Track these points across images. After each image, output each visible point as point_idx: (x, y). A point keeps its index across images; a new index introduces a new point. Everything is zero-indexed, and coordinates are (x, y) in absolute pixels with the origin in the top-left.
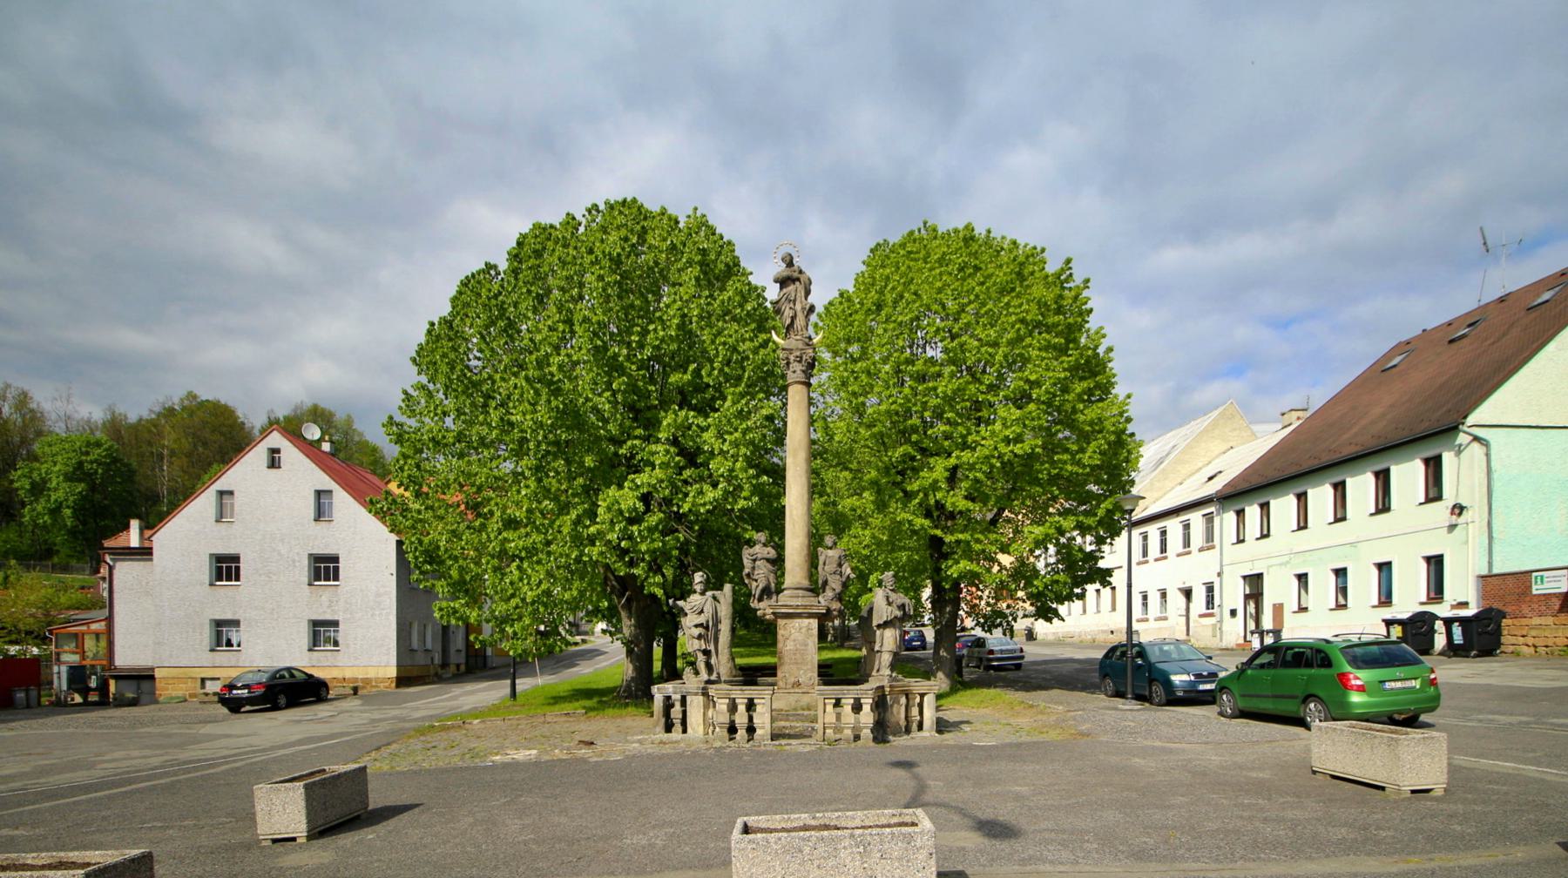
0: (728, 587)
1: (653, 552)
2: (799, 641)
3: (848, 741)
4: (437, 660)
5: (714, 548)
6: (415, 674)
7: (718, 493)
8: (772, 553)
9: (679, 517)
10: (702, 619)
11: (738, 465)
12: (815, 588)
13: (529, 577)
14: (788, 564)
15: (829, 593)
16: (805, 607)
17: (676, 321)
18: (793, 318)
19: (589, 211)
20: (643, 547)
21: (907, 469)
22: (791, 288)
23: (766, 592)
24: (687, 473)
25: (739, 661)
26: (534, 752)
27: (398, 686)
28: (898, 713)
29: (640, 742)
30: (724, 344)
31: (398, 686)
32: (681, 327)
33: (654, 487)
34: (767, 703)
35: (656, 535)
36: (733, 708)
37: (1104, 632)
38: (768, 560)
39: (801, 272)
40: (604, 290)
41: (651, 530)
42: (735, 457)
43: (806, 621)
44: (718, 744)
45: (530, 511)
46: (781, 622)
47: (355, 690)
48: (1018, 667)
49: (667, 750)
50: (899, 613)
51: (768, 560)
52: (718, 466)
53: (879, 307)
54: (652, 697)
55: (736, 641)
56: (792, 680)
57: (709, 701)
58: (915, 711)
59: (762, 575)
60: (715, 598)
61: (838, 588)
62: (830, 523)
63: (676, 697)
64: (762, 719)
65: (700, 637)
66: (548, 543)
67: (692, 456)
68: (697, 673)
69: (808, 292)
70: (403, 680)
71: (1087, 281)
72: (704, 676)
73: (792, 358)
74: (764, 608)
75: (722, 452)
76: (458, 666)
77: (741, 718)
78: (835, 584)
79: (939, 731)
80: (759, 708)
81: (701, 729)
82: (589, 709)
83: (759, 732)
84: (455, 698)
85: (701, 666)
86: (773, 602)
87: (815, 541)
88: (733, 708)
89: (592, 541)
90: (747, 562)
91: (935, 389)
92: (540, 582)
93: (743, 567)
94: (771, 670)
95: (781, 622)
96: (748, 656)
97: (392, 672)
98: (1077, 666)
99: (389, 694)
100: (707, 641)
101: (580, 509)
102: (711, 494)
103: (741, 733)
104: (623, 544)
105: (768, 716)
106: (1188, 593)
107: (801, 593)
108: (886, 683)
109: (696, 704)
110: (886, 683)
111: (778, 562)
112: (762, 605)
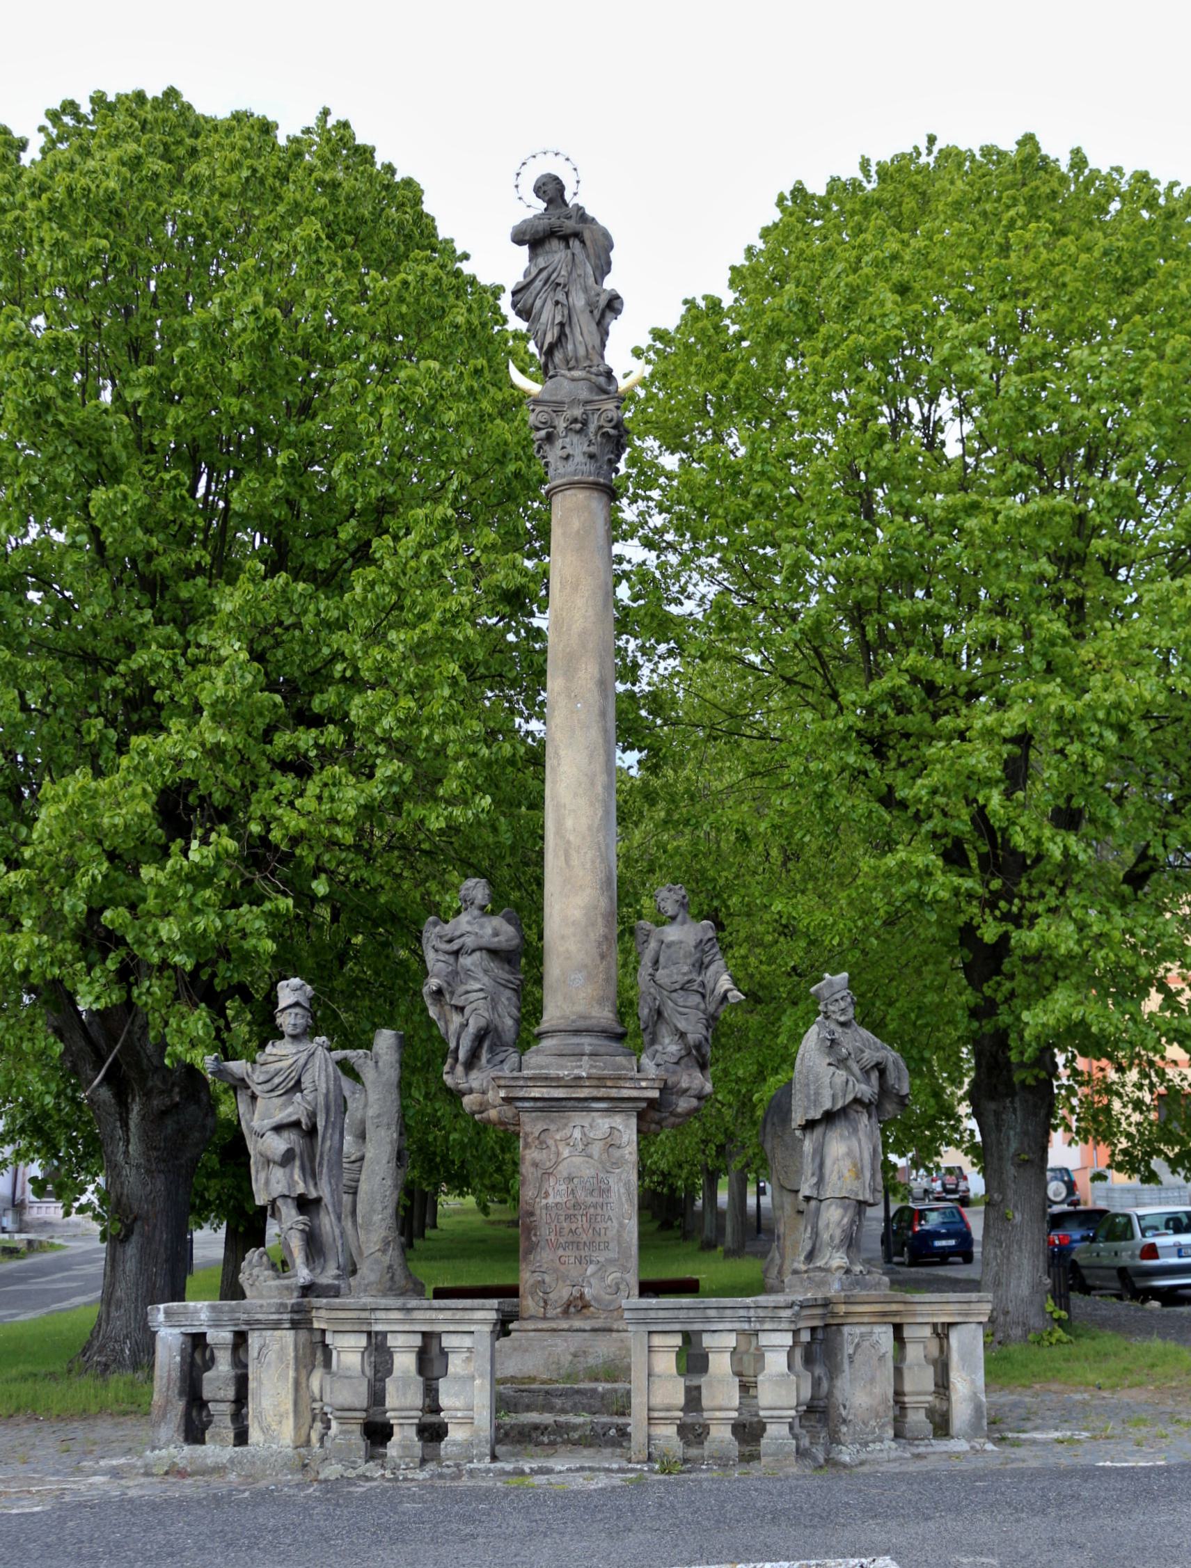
0: (385, 1039)
10: (295, 1110)
12: (628, 1027)
14: (554, 969)
16: (600, 1081)
29: (115, 1473)
38: (493, 953)
44: (332, 1471)
46: (531, 1126)
50: (867, 1090)
51: (493, 953)
56: (563, 1293)
59: (469, 998)
60: (346, 1068)
63: (220, 1337)
64: (467, 1400)
65: (287, 1159)
69: (604, 268)
73: (561, 424)
74: (481, 1089)
77: (403, 1398)
80: (456, 1364)
81: (286, 1433)
83: (456, 1434)
88: (378, 1349)
103: (404, 1437)
107: (587, 1043)
109: (273, 1355)
111: (523, 960)
112: (476, 1079)
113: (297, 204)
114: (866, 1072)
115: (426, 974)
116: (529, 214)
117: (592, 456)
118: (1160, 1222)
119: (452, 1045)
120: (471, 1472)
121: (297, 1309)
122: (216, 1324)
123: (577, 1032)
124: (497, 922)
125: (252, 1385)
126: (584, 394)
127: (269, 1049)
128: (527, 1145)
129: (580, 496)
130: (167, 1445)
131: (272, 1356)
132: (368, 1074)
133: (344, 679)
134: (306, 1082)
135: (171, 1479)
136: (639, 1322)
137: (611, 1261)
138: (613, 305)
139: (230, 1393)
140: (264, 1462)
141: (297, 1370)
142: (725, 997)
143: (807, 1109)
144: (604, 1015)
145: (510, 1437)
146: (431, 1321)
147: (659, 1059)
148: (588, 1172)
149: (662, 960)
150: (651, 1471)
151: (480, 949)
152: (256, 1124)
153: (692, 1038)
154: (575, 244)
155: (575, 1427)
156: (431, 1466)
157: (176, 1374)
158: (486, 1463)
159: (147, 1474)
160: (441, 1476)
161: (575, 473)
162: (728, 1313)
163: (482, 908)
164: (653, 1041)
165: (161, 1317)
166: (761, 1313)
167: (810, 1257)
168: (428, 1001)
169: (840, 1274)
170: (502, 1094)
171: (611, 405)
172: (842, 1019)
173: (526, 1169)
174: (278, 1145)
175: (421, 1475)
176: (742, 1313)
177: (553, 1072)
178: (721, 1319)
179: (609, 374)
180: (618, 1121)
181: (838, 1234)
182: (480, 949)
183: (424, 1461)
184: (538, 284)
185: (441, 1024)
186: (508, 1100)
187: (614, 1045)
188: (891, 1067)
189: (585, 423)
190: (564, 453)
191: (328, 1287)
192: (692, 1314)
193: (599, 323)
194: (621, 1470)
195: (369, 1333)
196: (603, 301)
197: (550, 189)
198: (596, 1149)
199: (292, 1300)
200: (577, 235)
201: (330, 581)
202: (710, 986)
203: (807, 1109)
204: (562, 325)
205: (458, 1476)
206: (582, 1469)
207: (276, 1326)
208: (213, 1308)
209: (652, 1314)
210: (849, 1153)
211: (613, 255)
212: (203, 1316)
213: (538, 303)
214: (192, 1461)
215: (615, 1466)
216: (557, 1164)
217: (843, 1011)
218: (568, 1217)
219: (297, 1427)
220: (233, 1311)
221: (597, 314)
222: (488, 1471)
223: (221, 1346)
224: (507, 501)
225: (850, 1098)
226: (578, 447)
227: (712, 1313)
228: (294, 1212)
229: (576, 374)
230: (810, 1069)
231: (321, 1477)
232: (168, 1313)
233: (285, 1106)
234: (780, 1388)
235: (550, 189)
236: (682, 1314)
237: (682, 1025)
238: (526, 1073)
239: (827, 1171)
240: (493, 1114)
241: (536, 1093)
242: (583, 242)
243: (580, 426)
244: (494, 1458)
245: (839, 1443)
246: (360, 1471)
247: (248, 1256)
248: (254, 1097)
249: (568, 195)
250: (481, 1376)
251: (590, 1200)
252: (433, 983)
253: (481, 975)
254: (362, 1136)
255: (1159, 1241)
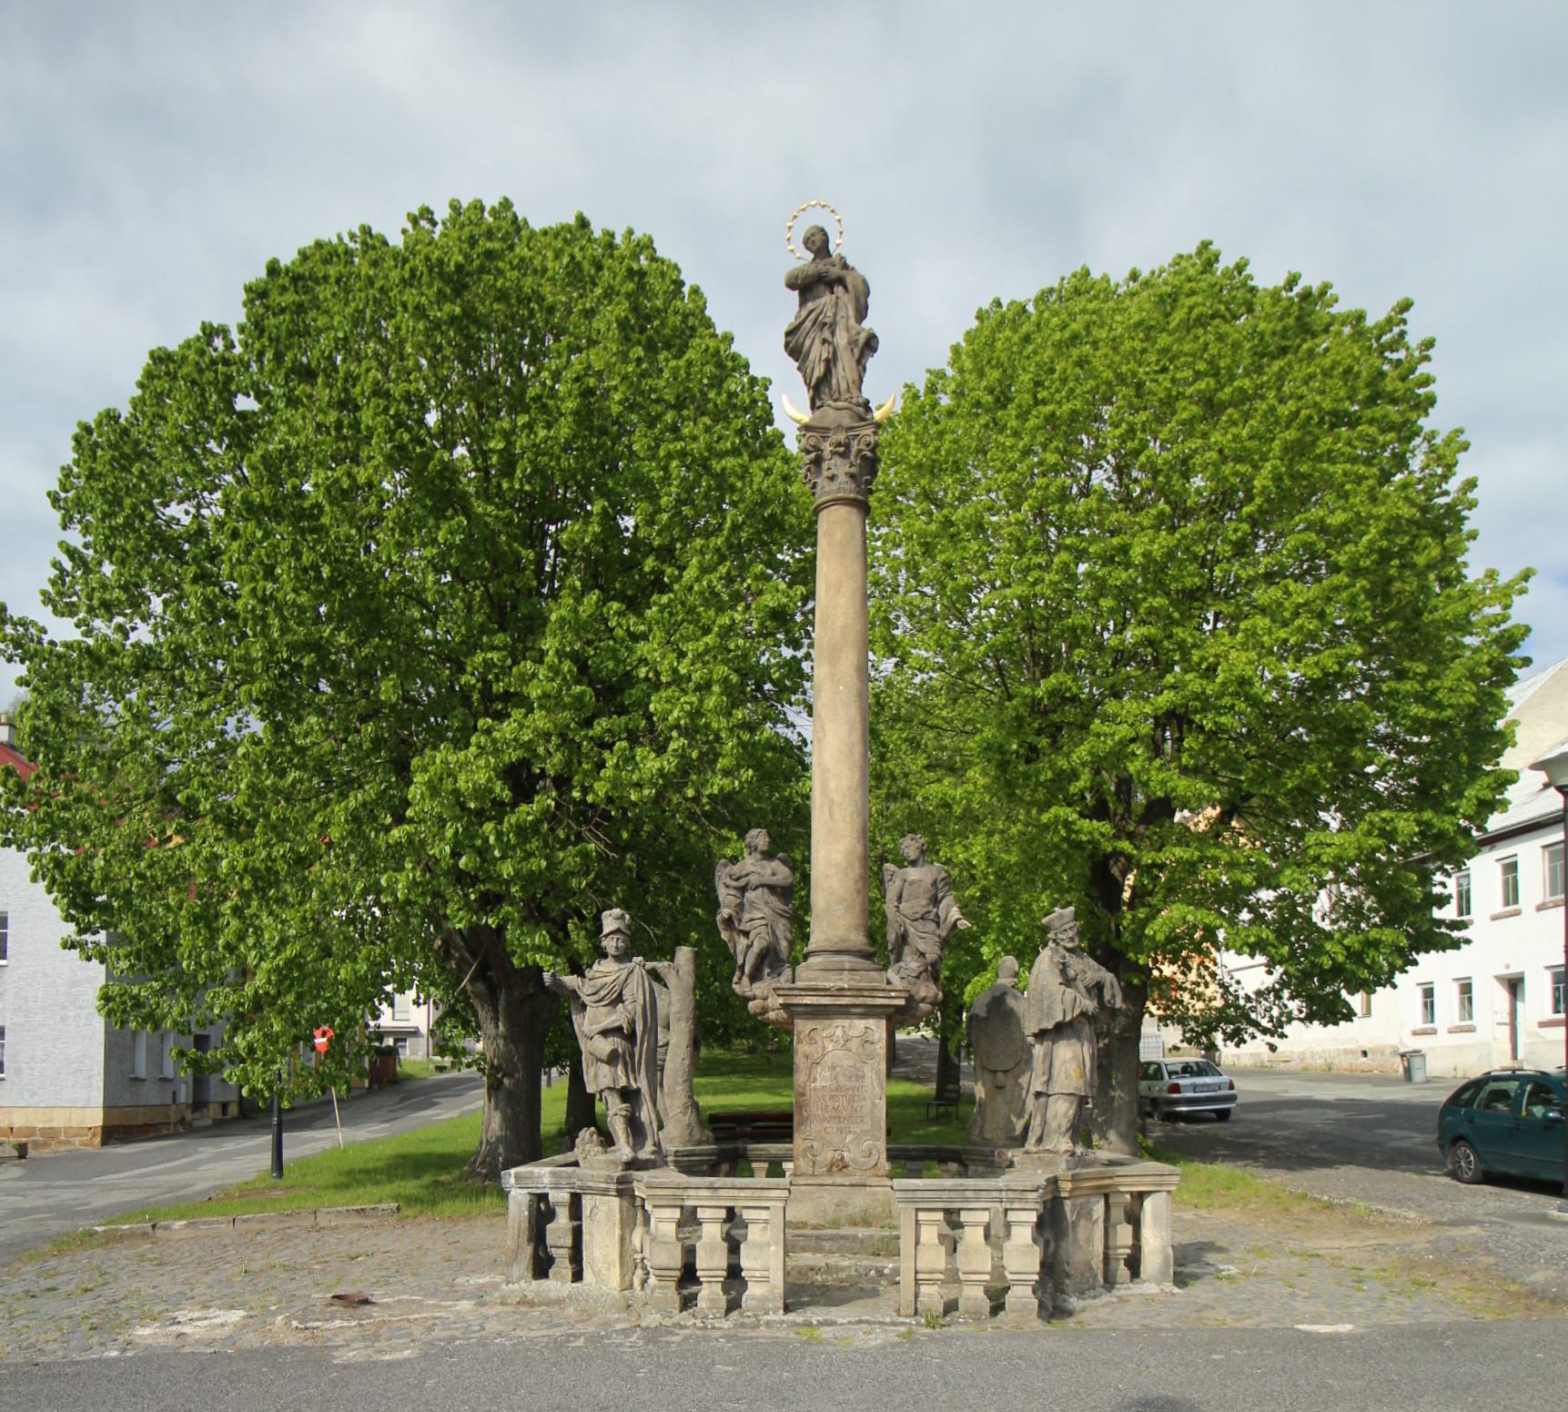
0: (684, 954)
1: (529, 880)
2: (845, 1071)
3: (975, 1315)
4: (185, 1096)
5: (661, 875)
6: (141, 1121)
7: (669, 763)
8: (778, 872)
9: (584, 813)
10: (618, 1017)
11: (711, 702)
12: (879, 945)
13: (259, 932)
14: (819, 899)
15: (911, 963)
16: (859, 991)
17: (570, 405)
18: (830, 363)
19: (415, 221)
20: (507, 869)
21: (1055, 721)
22: (827, 299)
23: (769, 960)
24: (601, 725)
25: (709, 1101)
26: (236, 1316)
27: (104, 1143)
28: (1087, 1243)
29: (480, 1297)
30: (683, 454)
31: (104, 1143)
32: (584, 417)
33: (528, 746)
34: (770, 1218)
35: (535, 844)
36: (689, 1219)
37: (1346, 1052)
38: (772, 888)
39: (845, 266)
40: (428, 334)
41: (523, 832)
42: (704, 687)
43: (860, 1024)
44: (652, 1319)
45: (256, 791)
46: (802, 1026)
47: (22, 1150)
48: (1223, 1115)
49: (534, 1331)
50: (1090, 1005)
51: (772, 888)
52: (669, 707)
53: (1003, 401)
54: (503, 1194)
55: (700, 1067)
56: (829, 1155)
57: (634, 1211)
58: (1124, 1234)
59: (760, 922)
60: (655, 975)
61: (932, 953)
62: (895, 820)
63: (560, 1197)
64: (765, 1262)
65: (612, 1059)
66: (302, 862)
67: (613, 691)
68: (607, 1140)
69: (862, 313)
70: (114, 1132)
71: (1429, 344)
72: (624, 1150)
73: (827, 448)
74: (764, 996)
75: (678, 680)
76: (225, 1106)
77: (711, 1260)
78: (925, 942)
79: (1180, 1280)
80: (754, 1233)
81: (614, 1277)
82: (411, 1200)
83: (754, 1290)
84: (194, 1166)
85: (618, 1128)
86: (783, 981)
87: (875, 863)
88: (689, 1219)
89: (395, 858)
90: (724, 894)
91: (1124, 550)
92: (283, 942)
93: (714, 904)
94: (779, 1126)
95: (802, 1026)
96: (727, 1092)
97: (96, 1118)
98: (1332, 1114)
99: (90, 1156)
100: (631, 1068)
101: (370, 791)
102: (651, 764)
103: (710, 1292)
104: (463, 862)
105: (776, 1251)
106: (1514, 985)
107: (847, 961)
108: (1061, 1169)
109: (603, 1215)
110: (1061, 1169)
111: (794, 898)
112: (759, 988)
113: (611, 287)
114: (1088, 990)
115: (718, 906)
116: (800, 264)
117: (852, 476)
118: (1179, 1068)
119: (740, 961)
120: (768, 1324)
121: (620, 1181)
122: (556, 1187)
123: (839, 952)
124: (776, 864)
125: (585, 1237)
126: (847, 422)
127: (596, 967)
128: (800, 1041)
129: (842, 512)
130: (519, 1280)
131: (601, 1215)
132: (671, 980)
133: (647, 679)
134: (627, 995)
135: (523, 1309)
136: (907, 1201)
137: (865, 1132)
138: (870, 344)
139: (569, 1241)
140: (596, 1300)
141: (622, 1228)
142: (955, 925)
143: (1040, 1020)
144: (858, 940)
145: (798, 1294)
146: (734, 1198)
147: (903, 973)
148: (847, 1063)
149: (905, 895)
150: (918, 1324)
151: (763, 886)
152: (586, 1028)
153: (931, 957)
154: (839, 290)
155: (842, 1269)
156: (735, 1315)
157: (525, 1225)
158: (780, 1316)
159: (503, 1304)
160: (743, 1325)
161: (839, 490)
162: (984, 1194)
163: (763, 853)
164: (899, 959)
165: (512, 1180)
166: (1011, 1195)
167: (1040, 1140)
168: (721, 927)
169: (1066, 1157)
170: (781, 1001)
171: (869, 431)
172: (1070, 945)
173: (799, 1060)
174: (605, 1046)
175: (726, 1324)
176: (995, 1194)
177: (821, 984)
178: (978, 1200)
179: (866, 405)
180: (871, 1022)
181: (1065, 1124)
182: (763, 886)
183: (729, 1310)
184: (808, 324)
185: (730, 945)
186: (785, 1006)
187: (867, 963)
188: (1108, 985)
189: (848, 446)
190: (829, 474)
191: (647, 1161)
192: (953, 1194)
193: (859, 362)
194: (894, 1324)
195: (682, 1207)
196: (862, 338)
197: (819, 244)
198: (854, 1044)
199: (618, 1173)
200: (841, 281)
201: (635, 604)
202: (942, 916)
203: (1040, 1020)
204: (827, 361)
205: (756, 1326)
206: (860, 1322)
207: (604, 1192)
208: (554, 1174)
209: (919, 1194)
210: (1074, 1058)
211: (870, 300)
212: (546, 1181)
213: (808, 342)
214: (538, 1294)
215: (888, 1320)
216: (823, 1056)
217: (1072, 939)
218: (832, 1097)
219: (623, 1276)
220: (569, 1177)
221: (857, 352)
222: (782, 1322)
223: (561, 1204)
224: (779, 531)
225: (1077, 1012)
226: (840, 468)
227: (969, 1194)
228: (617, 1100)
229: (840, 404)
230: (1044, 987)
231: (643, 1324)
232: (517, 1177)
233: (609, 1014)
234: (1023, 1255)
235: (819, 244)
236: (944, 1195)
237: (922, 947)
238: (799, 984)
239: (1055, 1072)
240: (772, 1015)
241: (807, 1000)
242: (845, 288)
243: (843, 451)
244: (787, 1309)
245: (1063, 1292)
246: (676, 1319)
247: (581, 1134)
248: (584, 1006)
249: (831, 247)
250: (776, 1243)
251: (849, 1084)
252: (725, 912)
253: (762, 906)
254: (667, 1027)
255: (1181, 1082)
